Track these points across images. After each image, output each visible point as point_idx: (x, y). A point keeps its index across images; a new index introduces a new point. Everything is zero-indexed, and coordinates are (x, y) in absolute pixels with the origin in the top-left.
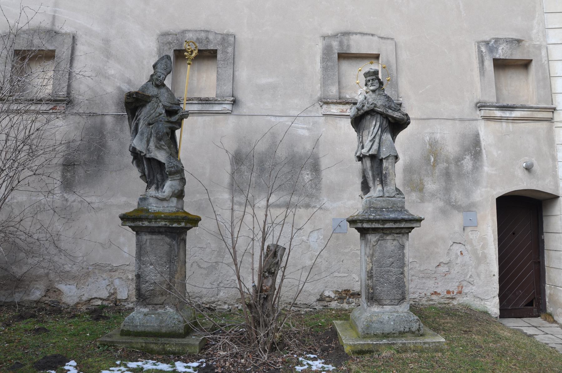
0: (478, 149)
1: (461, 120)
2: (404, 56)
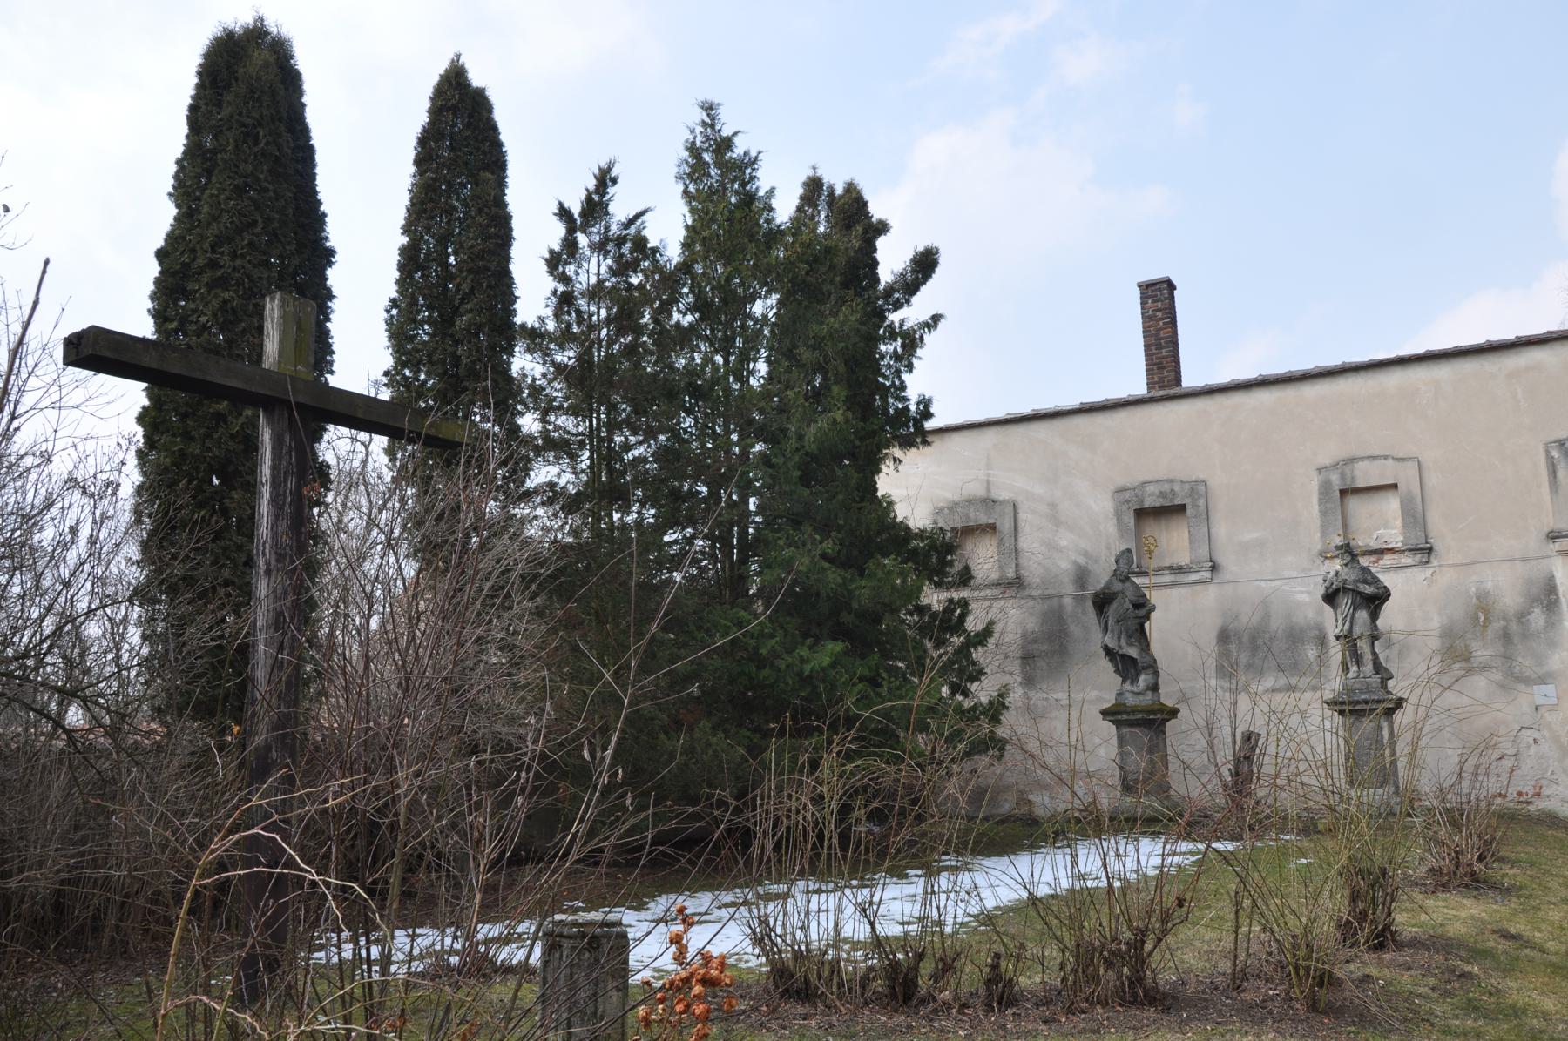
0: (1553, 597)
1: (1524, 559)
2: (1432, 480)
